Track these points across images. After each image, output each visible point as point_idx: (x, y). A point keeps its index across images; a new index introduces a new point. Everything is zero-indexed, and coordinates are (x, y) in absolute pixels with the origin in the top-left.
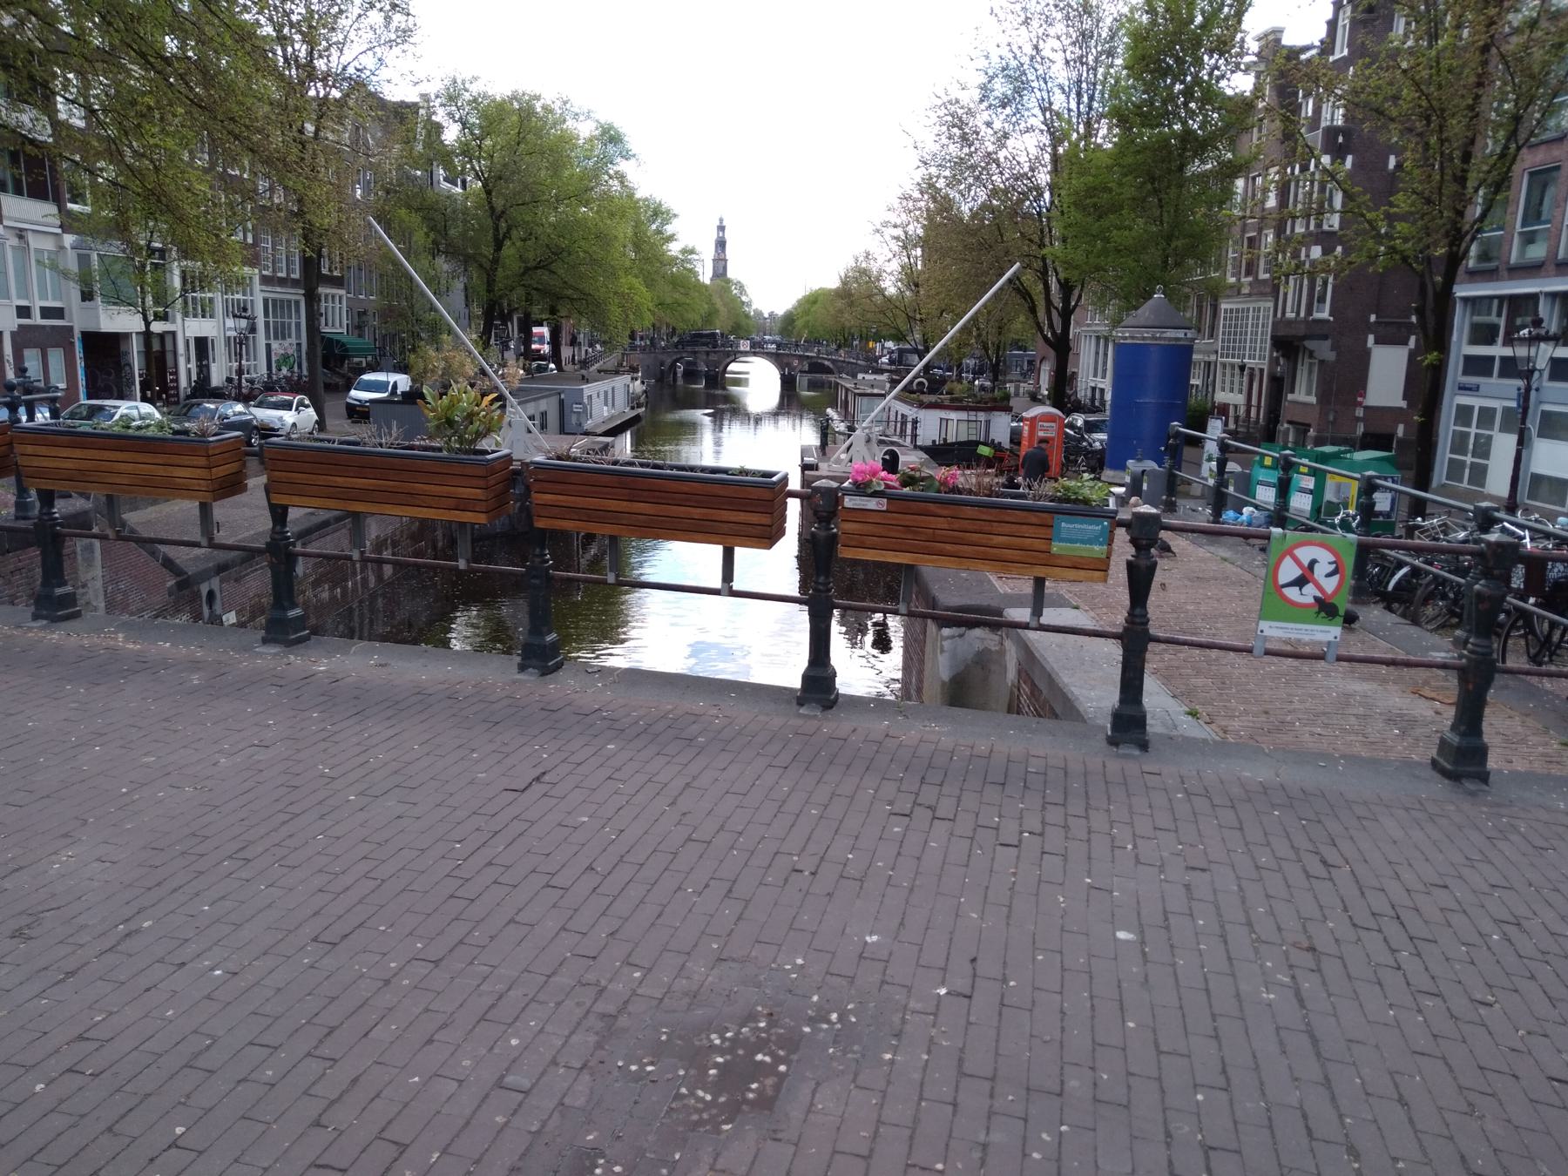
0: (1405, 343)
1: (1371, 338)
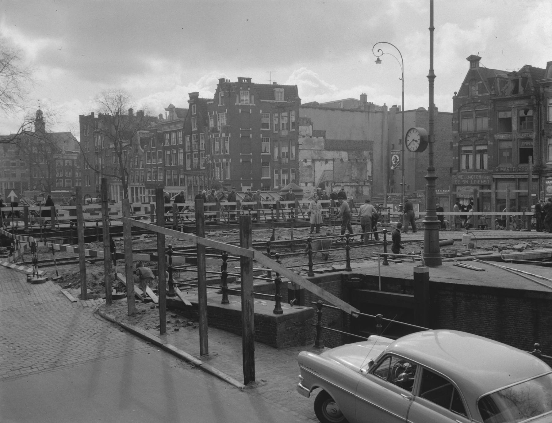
0: (250, 186)
1: (241, 184)
